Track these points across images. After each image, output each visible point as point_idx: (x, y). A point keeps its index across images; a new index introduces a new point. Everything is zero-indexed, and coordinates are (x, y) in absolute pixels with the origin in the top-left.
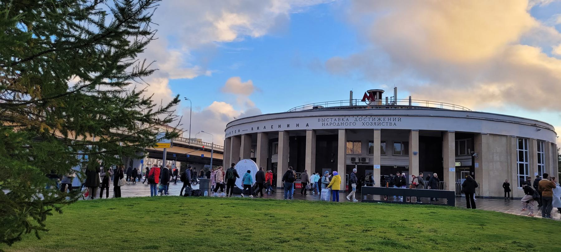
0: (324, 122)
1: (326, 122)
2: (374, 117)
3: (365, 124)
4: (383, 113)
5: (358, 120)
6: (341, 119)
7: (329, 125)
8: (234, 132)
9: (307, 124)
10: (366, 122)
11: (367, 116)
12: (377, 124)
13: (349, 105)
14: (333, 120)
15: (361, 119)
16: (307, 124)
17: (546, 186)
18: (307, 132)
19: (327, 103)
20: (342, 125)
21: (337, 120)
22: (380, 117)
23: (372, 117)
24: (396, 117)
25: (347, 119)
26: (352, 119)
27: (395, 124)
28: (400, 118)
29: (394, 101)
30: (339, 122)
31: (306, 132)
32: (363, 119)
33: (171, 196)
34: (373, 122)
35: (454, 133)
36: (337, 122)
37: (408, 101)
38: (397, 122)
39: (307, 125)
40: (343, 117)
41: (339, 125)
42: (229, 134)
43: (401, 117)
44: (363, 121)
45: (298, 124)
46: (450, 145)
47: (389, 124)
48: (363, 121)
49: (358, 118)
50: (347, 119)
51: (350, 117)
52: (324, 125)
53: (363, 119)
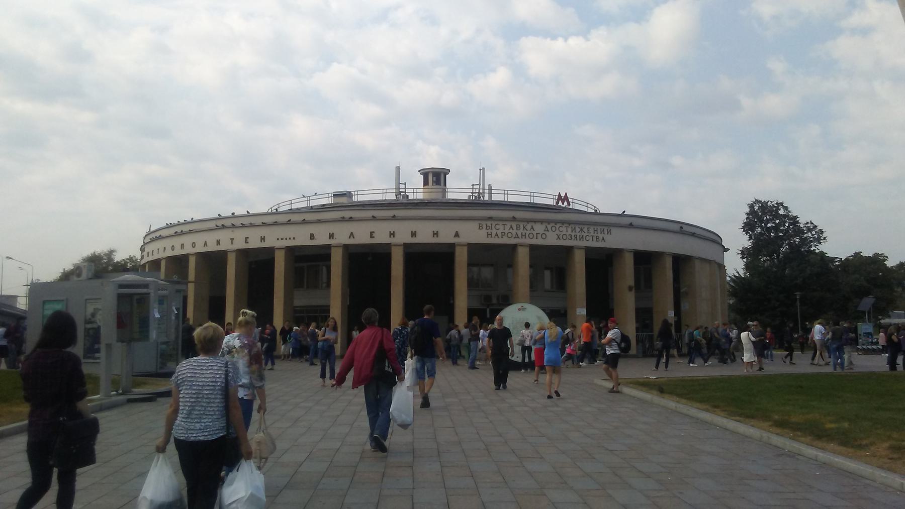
0: (489, 231)
1: (494, 232)
2: (573, 226)
3: (561, 237)
4: (692, 222)
5: (550, 230)
6: (522, 227)
7: (500, 235)
8: (162, 250)
9: (352, 234)
10: (562, 234)
11: (556, 222)
12: (578, 238)
13: (467, 199)
14: (507, 227)
15: (554, 229)
16: (352, 234)
17: (455, 363)
18: (229, 254)
19: (415, 190)
20: (524, 237)
21: (515, 227)
22: (583, 226)
23: (572, 225)
24: (604, 227)
25: (532, 228)
26: (539, 228)
27: (603, 239)
28: (575, 228)
29: (479, 193)
30: (517, 231)
31: (331, 250)
32: (557, 228)
33: (635, 334)
34: (573, 234)
35: (632, 254)
36: (514, 232)
37: (493, 191)
38: (607, 237)
39: (457, 235)
40: (525, 224)
41: (518, 238)
42: (150, 254)
43: (611, 228)
44: (557, 232)
45: (435, 236)
46: (626, 273)
47: (595, 239)
48: (557, 232)
49: (549, 227)
50: (532, 228)
51: (536, 223)
52: (489, 236)
53: (557, 228)
